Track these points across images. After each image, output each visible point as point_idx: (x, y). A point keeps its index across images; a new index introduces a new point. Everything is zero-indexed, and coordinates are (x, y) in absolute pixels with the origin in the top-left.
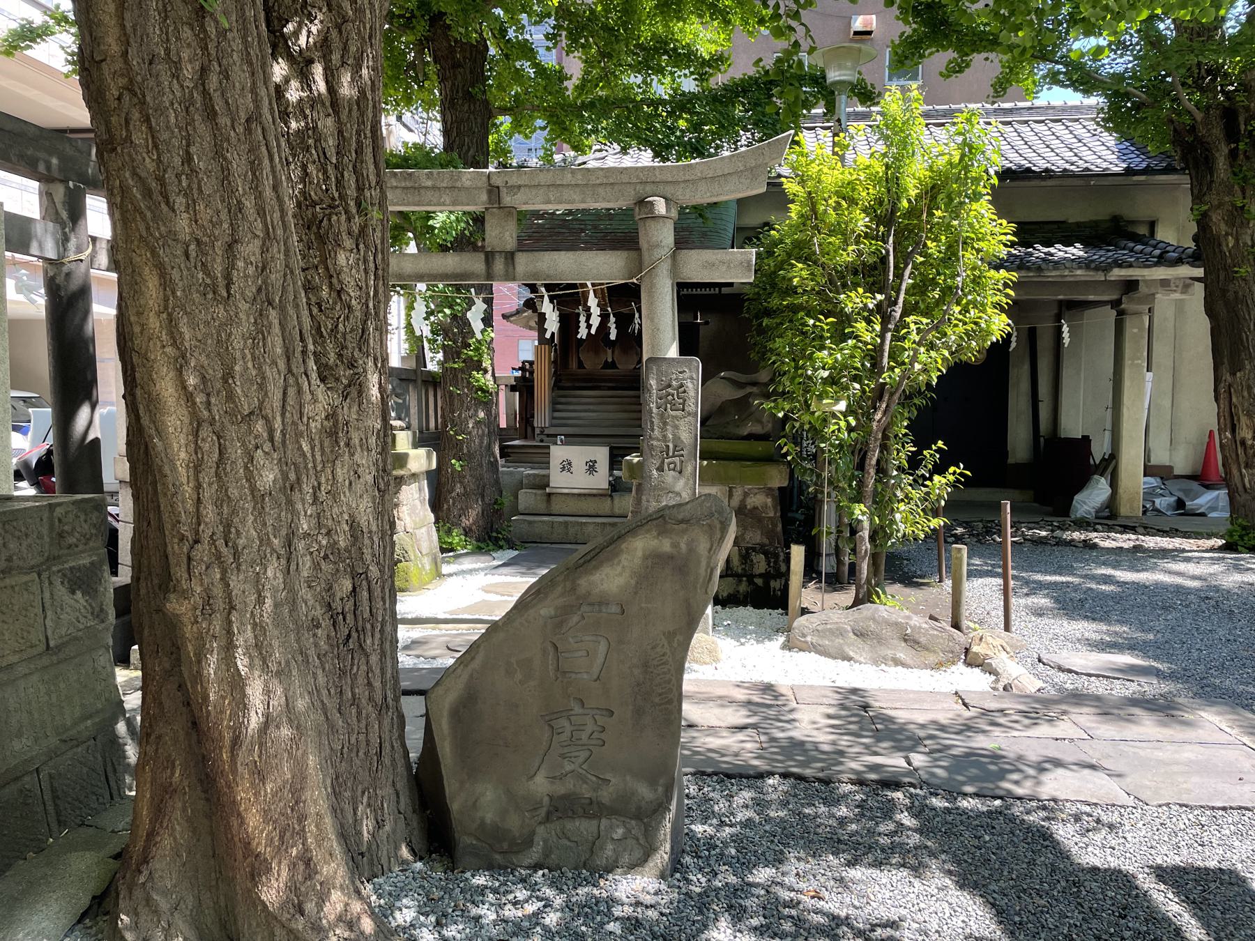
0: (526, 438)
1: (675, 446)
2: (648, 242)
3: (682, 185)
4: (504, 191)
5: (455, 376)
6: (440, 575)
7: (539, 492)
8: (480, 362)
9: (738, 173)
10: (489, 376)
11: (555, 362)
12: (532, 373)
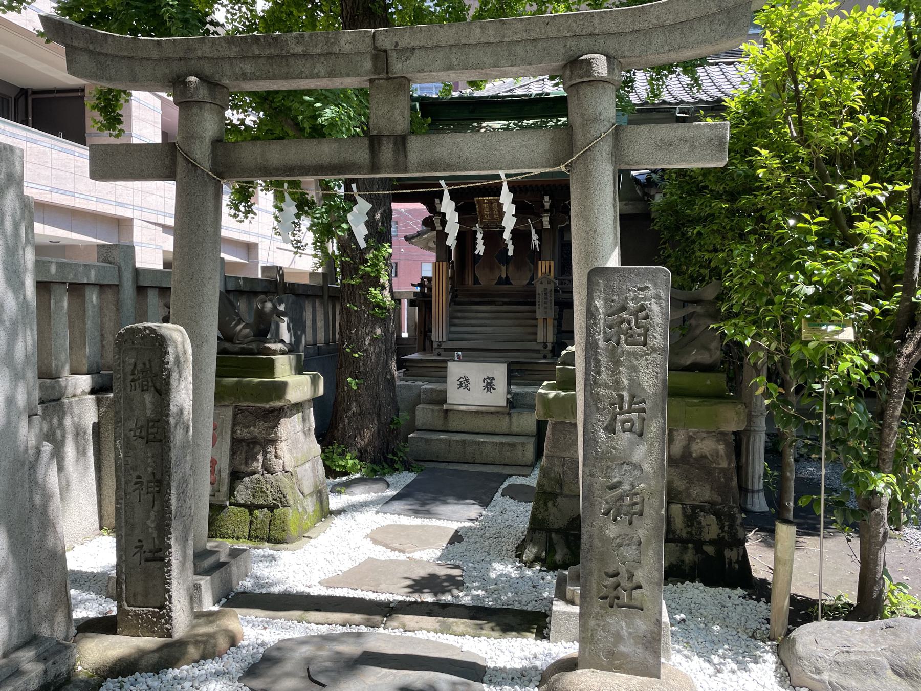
0: (424, 350)
1: (633, 397)
2: (583, 115)
4: (393, 55)
5: (353, 292)
6: (326, 513)
7: (437, 408)
8: (377, 278)
10: (386, 292)
11: (452, 278)
12: (430, 289)
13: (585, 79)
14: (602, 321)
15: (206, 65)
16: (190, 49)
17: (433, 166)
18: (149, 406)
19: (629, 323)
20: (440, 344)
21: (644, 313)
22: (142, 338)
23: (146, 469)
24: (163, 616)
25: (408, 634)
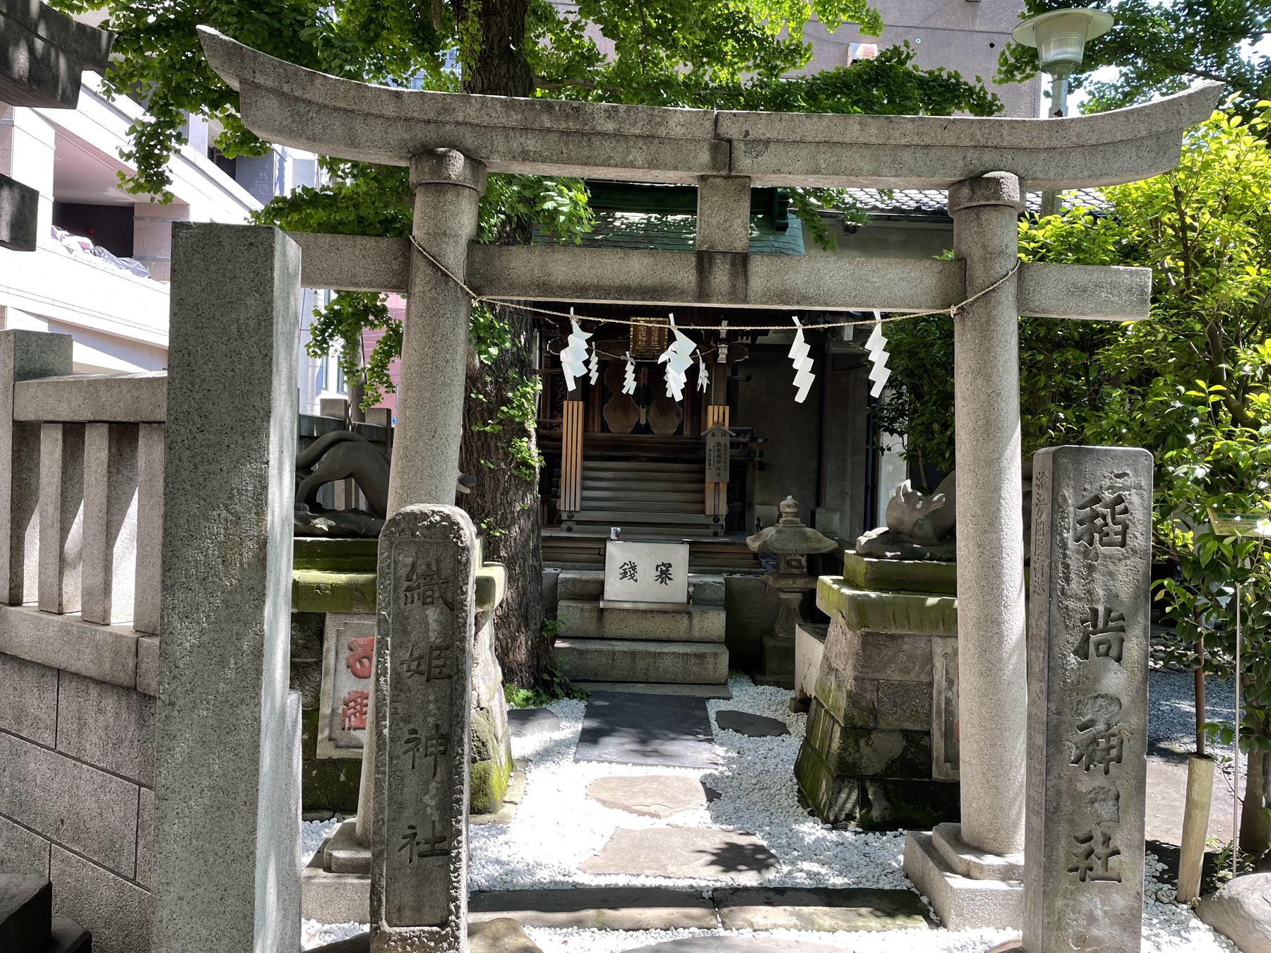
2: (985, 247)
3: (1043, 155)
4: (740, 148)
7: (587, 606)
9: (1136, 141)
13: (993, 202)
14: (1071, 516)
15: (468, 135)
16: (446, 110)
17: (783, 296)
18: (433, 626)
19: (1104, 518)
20: (571, 514)
21: (1122, 506)
22: (428, 527)
23: (425, 721)
24: (444, 938)
25: (761, 935)
